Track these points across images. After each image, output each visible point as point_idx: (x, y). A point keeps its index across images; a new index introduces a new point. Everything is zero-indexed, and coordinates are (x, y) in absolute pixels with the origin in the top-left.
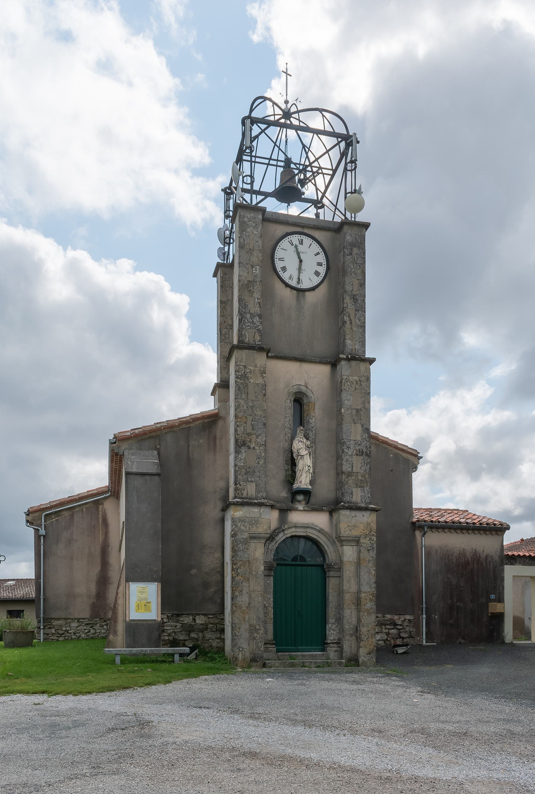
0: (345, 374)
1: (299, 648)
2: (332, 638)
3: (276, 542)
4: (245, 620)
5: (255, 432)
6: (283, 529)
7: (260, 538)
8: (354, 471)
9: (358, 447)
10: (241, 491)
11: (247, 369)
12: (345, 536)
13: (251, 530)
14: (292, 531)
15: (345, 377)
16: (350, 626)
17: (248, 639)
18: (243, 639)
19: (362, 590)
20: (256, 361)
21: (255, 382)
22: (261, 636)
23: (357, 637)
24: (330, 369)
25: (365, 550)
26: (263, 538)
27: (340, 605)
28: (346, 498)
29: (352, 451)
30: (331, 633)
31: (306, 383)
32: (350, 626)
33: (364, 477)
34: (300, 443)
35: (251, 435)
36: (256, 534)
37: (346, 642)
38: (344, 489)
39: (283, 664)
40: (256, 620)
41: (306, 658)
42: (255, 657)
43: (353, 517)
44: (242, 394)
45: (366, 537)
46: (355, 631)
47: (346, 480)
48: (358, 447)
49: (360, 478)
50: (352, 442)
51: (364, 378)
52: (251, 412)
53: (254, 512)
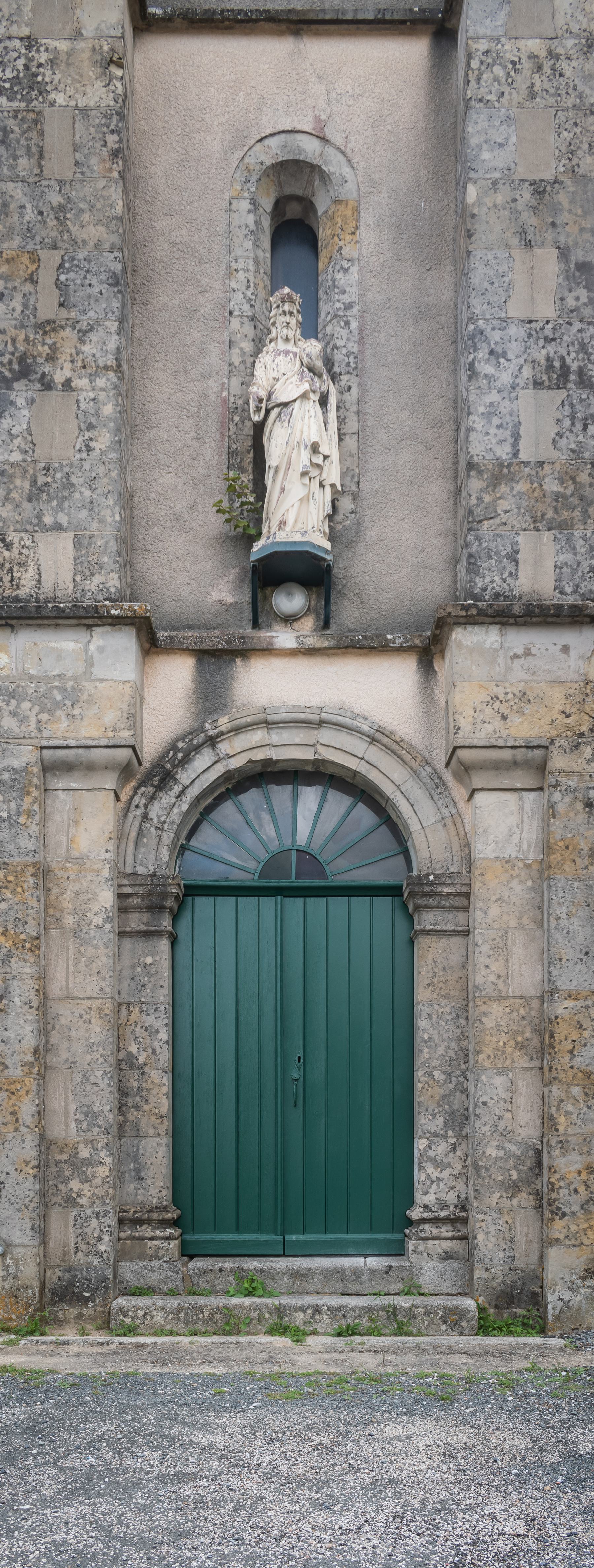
0: (481, 31)
1: (294, 1237)
2: (430, 1199)
3: (182, 792)
4: (17, 1120)
5: (73, 315)
6: (210, 733)
7: (90, 768)
8: (523, 456)
9: (544, 352)
10: (11, 570)
11: (38, 51)
12: (476, 742)
13: (46, 733)
14: (254, 744)
15: (483, 46)
16: (506, 1145)
17: (32, 1205)
18: (7, 1205)
19: (559, 983)
20: (78, 11)
21: (73, 103)
22: (100, 1192)
23: (538, 1196)
24: (426, 53)
25: (572, 803)
26: (107, 767)
27: (467, 1055)
28: (488, 579)
29: (513, 367)
30: (428, 1177)
31: (318, 119)
32: (506, 1145)
33: (573, 479)
34: (282, 357)
35: (54, 330)
36: (68, 747)
37: (489, 1219)
38: (478, 539)
39: (187, 1314)
40: (78, 1122)
41: (310, 1287)
42: (71, 1284)
43: (516, 656)
44: (15, 158)
45: (577, 746)
46: (531, 1169)
47: (487, 498)
48: (544, 352)
49: (552, 486)
50: (513, 330)
51: (570, 43)
52: (54, 234)
53: (60, 656)
